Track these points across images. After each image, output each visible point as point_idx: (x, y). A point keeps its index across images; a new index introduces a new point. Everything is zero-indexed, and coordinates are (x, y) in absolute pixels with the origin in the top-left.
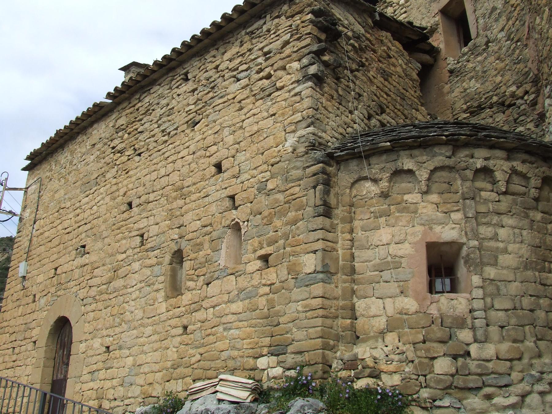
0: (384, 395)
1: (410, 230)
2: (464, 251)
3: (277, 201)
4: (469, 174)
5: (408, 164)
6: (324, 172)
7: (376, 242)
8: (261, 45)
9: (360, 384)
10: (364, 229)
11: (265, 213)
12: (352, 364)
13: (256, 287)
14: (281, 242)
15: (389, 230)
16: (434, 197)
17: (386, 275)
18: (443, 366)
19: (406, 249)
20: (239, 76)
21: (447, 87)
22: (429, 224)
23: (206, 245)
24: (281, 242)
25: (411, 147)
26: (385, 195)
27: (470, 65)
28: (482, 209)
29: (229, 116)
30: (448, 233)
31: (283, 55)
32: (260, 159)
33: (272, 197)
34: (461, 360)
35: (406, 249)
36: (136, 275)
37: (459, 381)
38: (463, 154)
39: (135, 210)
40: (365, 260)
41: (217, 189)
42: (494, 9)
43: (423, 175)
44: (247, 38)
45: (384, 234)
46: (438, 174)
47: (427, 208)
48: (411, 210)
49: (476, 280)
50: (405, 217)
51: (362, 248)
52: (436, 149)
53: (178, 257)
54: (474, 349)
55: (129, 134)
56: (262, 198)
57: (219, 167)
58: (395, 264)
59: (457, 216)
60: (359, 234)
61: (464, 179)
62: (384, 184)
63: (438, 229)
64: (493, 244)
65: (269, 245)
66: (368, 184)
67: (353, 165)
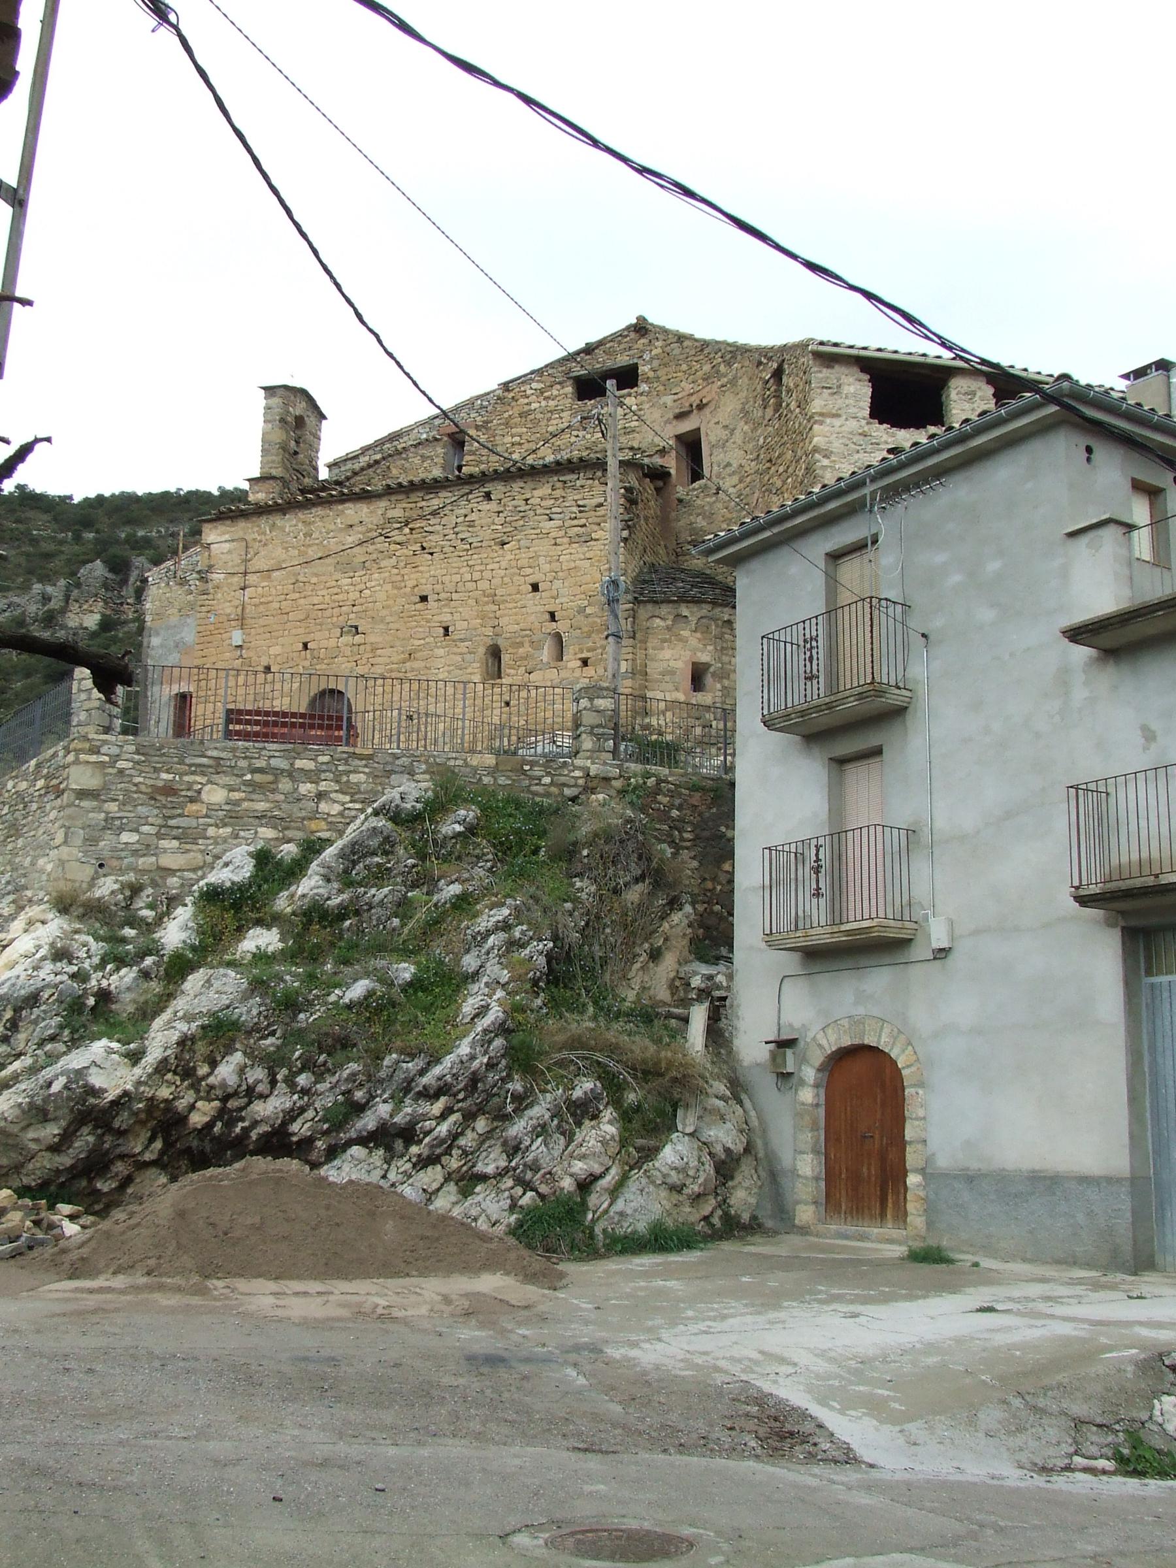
0: (667, 744)
1: (682, 653)
2: (712, 669)
3: (595, 622)
4: (720, 623)
5: (685, 611)
6: (633, 609)
7: (661, 657)
8: (576, 498)
9: (654, 737)
10: (654, 649)
11: (586, 629)
12: (646, 727)
13: (578, 678)
14: (600, 651)
15: (671, 652)
16: (698, 635)
17: (667, 678)
18: (698, 731)
19: (679, 664)
20: (553, 516)
21: (673, 514)
22: (694, 651)
23: (527, 644)
24: (600, 651)
25: (689, 602)
26: (668, 628)
27: (699, 502)
28: (725, 645)
29: (543, 547)
30: (704, 657)
31: (598, 514)
32: (578, 590)
33: (590, 620)
34: (707, 729)
35: (679, 664)
36: (443, 660)
37: (706, 740)
38: (718, 610)
39: (431, 603)
40: (654, 669)
41: (536, 606)
42: (729, 464)
43: (693, 620)
44: (559, 485)
45: (667, 654)
46: (704, 620)
47: (694, 640)
48: (684, 640)
49: (719, 686)
50: (681, 644)
51: (652, 660)
52: (703, 605)
53: (495, 653)
54: (714, 724)
55: (411, 529)
56: (580, 618)
57: (535, 587)
58: (672, 673)
59: (710, 648)
60: (651, 651)
61: (717, 626)
62: (669, 622)
63: (699, 654)
64: (728, 667)
65: (588, 651)
66: (658, 620)
67: (650, 607)
